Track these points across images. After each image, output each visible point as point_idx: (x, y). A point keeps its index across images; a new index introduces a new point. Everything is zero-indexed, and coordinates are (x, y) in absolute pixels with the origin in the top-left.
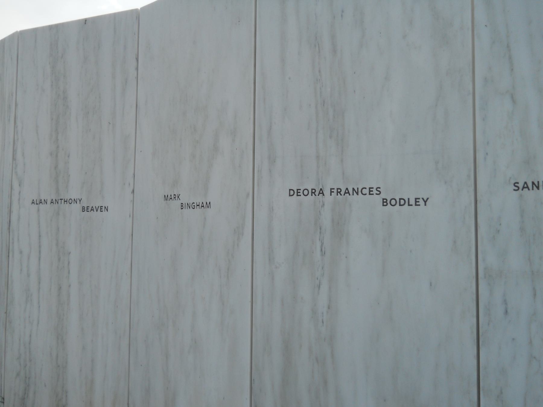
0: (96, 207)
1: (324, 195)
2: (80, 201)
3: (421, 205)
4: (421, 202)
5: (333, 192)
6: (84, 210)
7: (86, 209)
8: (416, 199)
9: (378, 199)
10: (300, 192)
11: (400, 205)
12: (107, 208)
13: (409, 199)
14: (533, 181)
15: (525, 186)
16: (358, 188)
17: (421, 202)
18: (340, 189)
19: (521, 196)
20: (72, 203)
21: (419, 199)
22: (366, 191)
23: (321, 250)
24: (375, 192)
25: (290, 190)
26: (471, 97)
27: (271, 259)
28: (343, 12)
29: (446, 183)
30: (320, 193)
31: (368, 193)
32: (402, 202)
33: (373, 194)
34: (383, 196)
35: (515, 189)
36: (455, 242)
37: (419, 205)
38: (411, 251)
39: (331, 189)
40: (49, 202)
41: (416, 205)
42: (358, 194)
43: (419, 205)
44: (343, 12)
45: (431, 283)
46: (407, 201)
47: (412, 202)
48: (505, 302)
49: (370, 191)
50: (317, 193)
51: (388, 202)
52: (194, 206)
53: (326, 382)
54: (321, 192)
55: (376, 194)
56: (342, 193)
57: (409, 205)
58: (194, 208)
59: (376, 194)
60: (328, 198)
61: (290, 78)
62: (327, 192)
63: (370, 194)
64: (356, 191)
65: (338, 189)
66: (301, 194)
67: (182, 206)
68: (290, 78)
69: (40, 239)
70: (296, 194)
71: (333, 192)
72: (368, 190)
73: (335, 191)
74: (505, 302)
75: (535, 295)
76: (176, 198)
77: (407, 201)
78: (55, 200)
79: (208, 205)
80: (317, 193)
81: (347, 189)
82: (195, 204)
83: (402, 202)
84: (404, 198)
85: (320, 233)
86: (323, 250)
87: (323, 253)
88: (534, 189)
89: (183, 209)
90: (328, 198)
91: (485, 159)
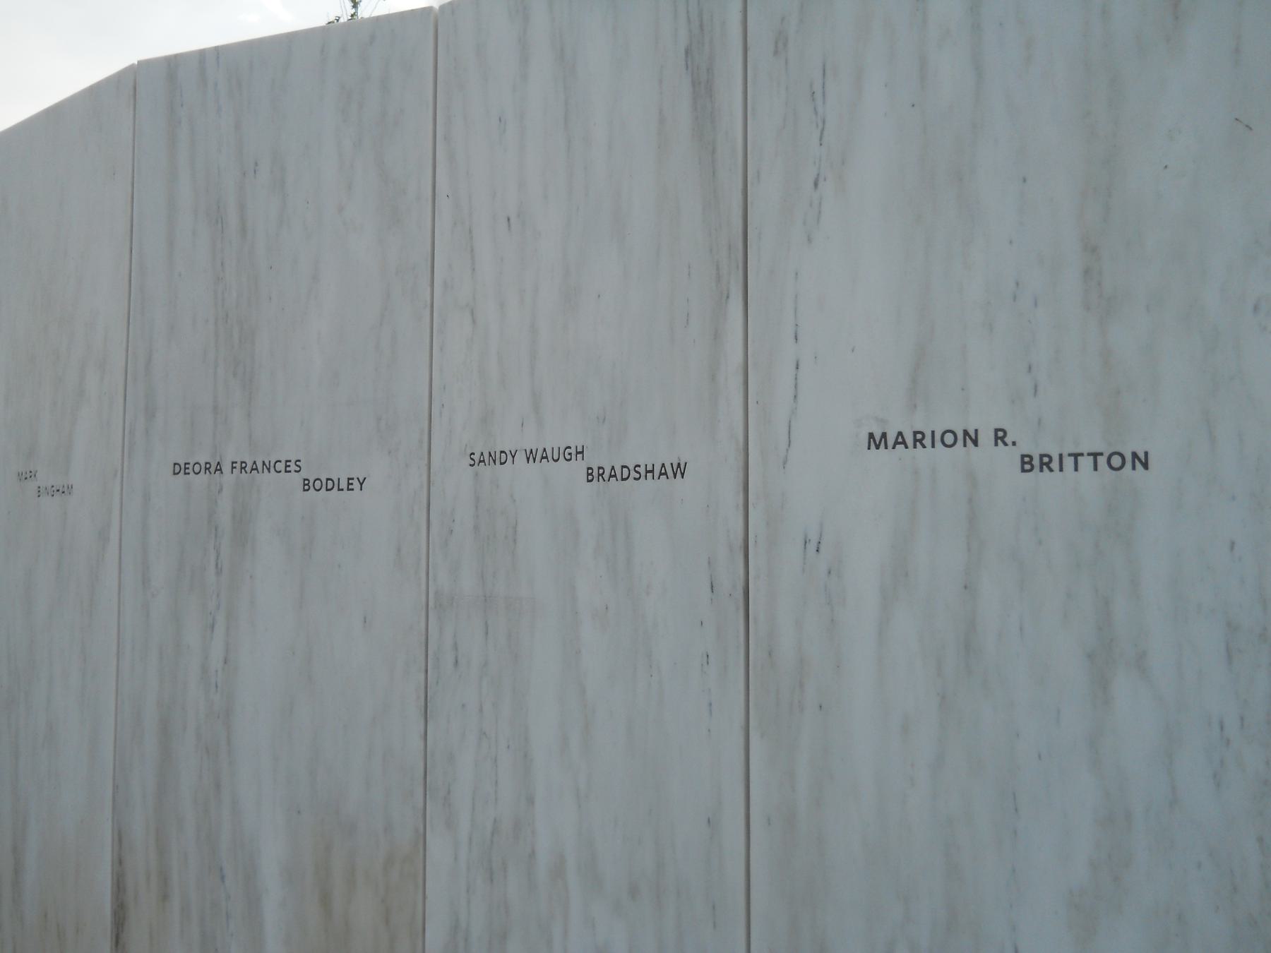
0: (672, 464)
1: (222, 473)
2: (513, 457)
3: (976, 428)
4: (356, 485)
5: (235, 468)
6: (590, 477)
7: (597, 475)
8: (349, 479)
9: (296, 479)
10: (188, 468)
11: (327, 490)
12: (534, 454)
13: (339, 479)
14: (1134, 450)
15: (899, 441)
16: (270, 462)
17: (356, 485)
18: (245, 462)
19: (477, 474)
20: (314, 482)
21: (353, 479)
22: (280, 466)
23: (217, 565)
24: (293, 467)
25: (175, 464)
26: (428, 310)
27: (145, 581)
28: (256, 164)
29: (390, 452)
30: (216, 470)
31: (283, 470)
32: (330, 485)
33: (290, 471)
34: (304, 474)
35: (962, 444)
36: (399, 550)
37: (353, 490)
38: (339, 566)
39: (349, 479)
40: (1085, 454)
41: (348, 489)
42: (269, 472)
43: (353, 490)
44: (256, 164)
45: (365, 618)
46: (336, 483)
47: (344, 485)
48: (456, 647)
49: (286, 466)
50: (212, 469)
51: (311, 484)
52: (570, 454)
53: (218, 786)
54: (219, 469)
55: (296, 471)
56: (248, 469)
57: (339, 490)
58: (571, 459)
59: (296, 471)
60: (228, 478)
61: (180, 275)
62: (226, 468)
63: (286, 471)
64: (267, 467)
65: (242, 463)
66: (190, 471)
67: (588, 474)
68: (180, 275)
69: (823, 88)
70: (182, 471)
71: (235, 468)
72: (283, 463)
73: (238, 465)
74: (456, 647)
75: (487, 633)
76: (246, 469)
77: (336, 483)
78: (677, 464)
79: (70, 487)
80: (212, 469)
81: (255, 463)
82: (573, 451)
83: (330, 485)
84: (1124, 454)
85: (216, 536)
86: (219, 566)
87: (219, 571)
88: (974, 431)
89: (592, 480)
90: (228, 478)
91: (441, 413)
